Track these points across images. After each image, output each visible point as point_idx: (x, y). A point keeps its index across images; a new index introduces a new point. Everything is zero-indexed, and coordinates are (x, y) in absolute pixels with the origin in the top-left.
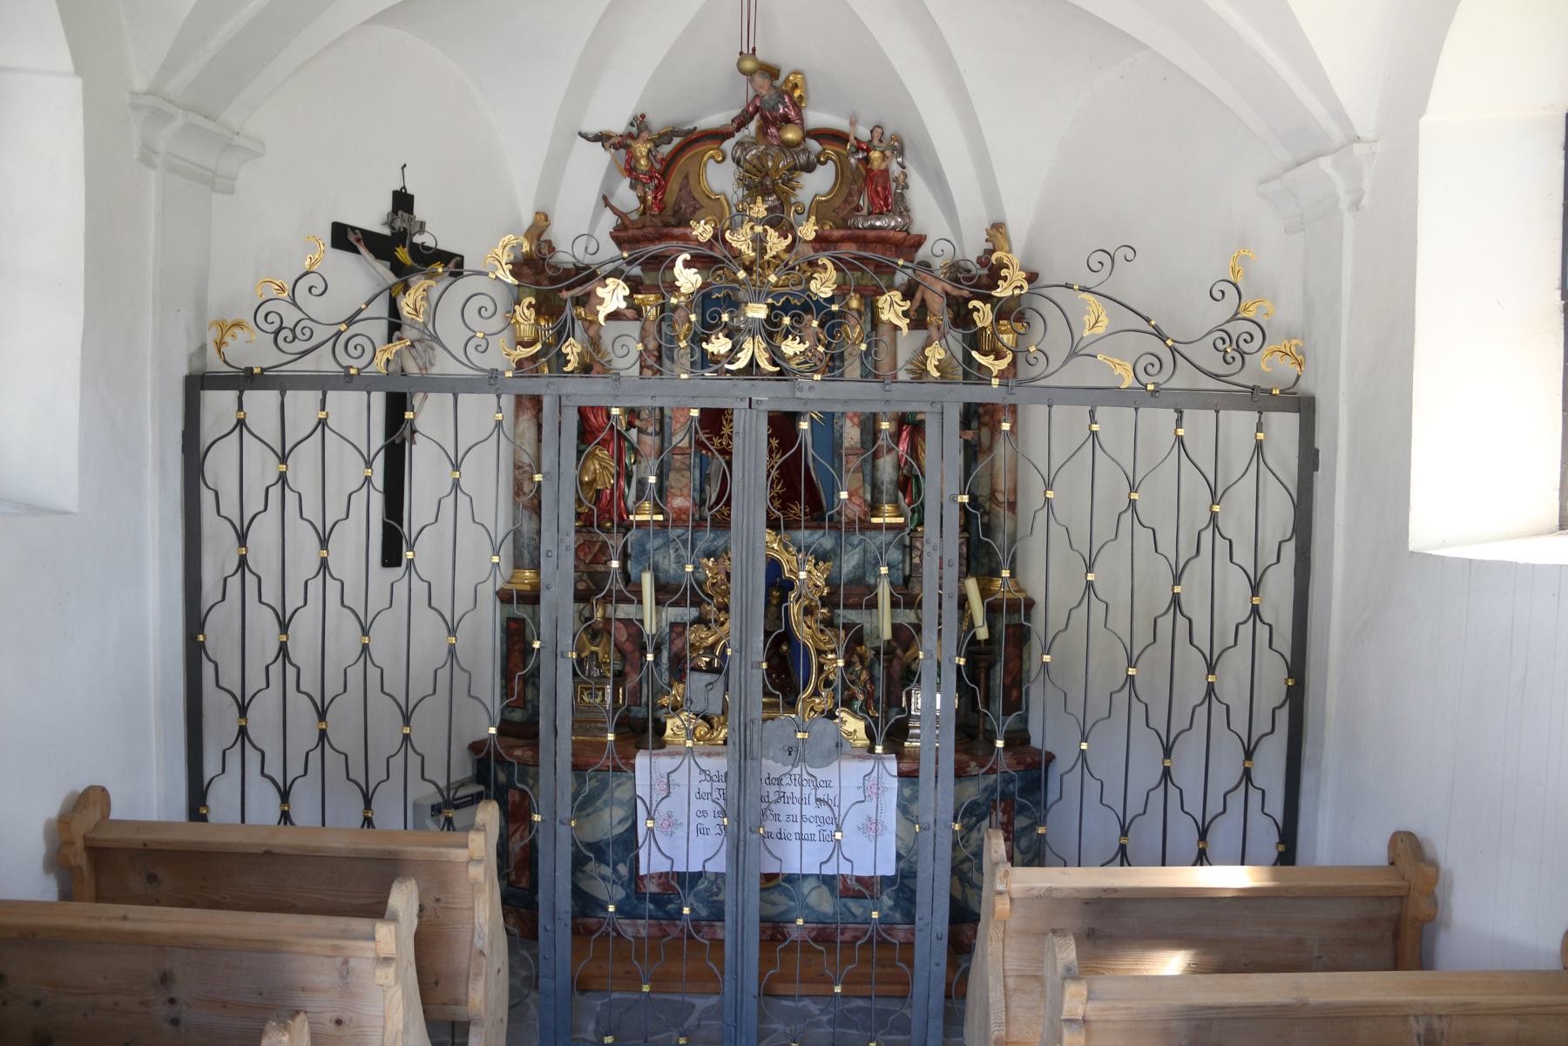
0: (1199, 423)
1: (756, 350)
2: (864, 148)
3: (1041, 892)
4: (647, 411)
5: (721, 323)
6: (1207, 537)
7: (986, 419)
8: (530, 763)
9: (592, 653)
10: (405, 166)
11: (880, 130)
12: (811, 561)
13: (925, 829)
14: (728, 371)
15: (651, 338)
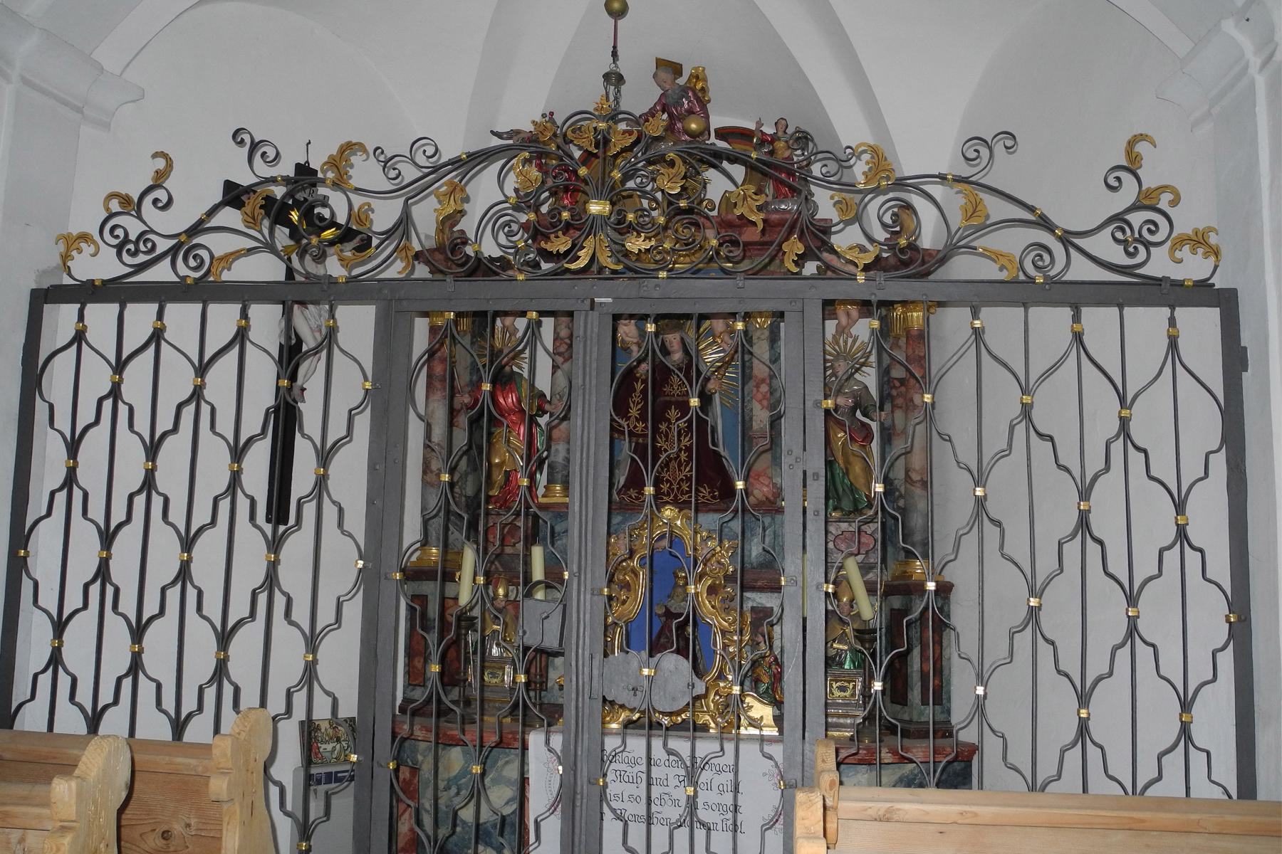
0: (1100, 321)
1: (598, 247)
2: (766, 141)
3: (880, 813)
4: (558, 396)
5: (561, 222)
6: (1117, 447)
7: (900, 401)
8: (420, 738)
9: (494, 631)
10: (309, 143)
11: (783, 122)
12: (715, 539)
13: (791, 787)
14: (568, 270)
15: (563, 326)
